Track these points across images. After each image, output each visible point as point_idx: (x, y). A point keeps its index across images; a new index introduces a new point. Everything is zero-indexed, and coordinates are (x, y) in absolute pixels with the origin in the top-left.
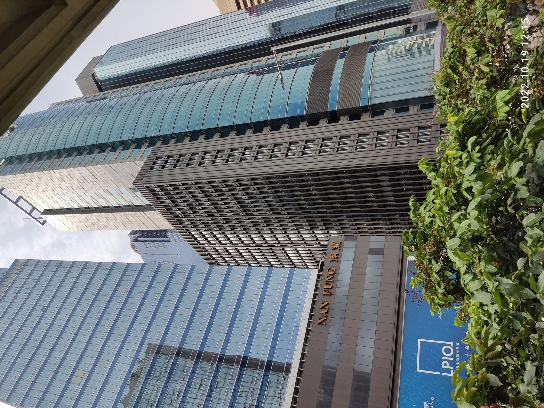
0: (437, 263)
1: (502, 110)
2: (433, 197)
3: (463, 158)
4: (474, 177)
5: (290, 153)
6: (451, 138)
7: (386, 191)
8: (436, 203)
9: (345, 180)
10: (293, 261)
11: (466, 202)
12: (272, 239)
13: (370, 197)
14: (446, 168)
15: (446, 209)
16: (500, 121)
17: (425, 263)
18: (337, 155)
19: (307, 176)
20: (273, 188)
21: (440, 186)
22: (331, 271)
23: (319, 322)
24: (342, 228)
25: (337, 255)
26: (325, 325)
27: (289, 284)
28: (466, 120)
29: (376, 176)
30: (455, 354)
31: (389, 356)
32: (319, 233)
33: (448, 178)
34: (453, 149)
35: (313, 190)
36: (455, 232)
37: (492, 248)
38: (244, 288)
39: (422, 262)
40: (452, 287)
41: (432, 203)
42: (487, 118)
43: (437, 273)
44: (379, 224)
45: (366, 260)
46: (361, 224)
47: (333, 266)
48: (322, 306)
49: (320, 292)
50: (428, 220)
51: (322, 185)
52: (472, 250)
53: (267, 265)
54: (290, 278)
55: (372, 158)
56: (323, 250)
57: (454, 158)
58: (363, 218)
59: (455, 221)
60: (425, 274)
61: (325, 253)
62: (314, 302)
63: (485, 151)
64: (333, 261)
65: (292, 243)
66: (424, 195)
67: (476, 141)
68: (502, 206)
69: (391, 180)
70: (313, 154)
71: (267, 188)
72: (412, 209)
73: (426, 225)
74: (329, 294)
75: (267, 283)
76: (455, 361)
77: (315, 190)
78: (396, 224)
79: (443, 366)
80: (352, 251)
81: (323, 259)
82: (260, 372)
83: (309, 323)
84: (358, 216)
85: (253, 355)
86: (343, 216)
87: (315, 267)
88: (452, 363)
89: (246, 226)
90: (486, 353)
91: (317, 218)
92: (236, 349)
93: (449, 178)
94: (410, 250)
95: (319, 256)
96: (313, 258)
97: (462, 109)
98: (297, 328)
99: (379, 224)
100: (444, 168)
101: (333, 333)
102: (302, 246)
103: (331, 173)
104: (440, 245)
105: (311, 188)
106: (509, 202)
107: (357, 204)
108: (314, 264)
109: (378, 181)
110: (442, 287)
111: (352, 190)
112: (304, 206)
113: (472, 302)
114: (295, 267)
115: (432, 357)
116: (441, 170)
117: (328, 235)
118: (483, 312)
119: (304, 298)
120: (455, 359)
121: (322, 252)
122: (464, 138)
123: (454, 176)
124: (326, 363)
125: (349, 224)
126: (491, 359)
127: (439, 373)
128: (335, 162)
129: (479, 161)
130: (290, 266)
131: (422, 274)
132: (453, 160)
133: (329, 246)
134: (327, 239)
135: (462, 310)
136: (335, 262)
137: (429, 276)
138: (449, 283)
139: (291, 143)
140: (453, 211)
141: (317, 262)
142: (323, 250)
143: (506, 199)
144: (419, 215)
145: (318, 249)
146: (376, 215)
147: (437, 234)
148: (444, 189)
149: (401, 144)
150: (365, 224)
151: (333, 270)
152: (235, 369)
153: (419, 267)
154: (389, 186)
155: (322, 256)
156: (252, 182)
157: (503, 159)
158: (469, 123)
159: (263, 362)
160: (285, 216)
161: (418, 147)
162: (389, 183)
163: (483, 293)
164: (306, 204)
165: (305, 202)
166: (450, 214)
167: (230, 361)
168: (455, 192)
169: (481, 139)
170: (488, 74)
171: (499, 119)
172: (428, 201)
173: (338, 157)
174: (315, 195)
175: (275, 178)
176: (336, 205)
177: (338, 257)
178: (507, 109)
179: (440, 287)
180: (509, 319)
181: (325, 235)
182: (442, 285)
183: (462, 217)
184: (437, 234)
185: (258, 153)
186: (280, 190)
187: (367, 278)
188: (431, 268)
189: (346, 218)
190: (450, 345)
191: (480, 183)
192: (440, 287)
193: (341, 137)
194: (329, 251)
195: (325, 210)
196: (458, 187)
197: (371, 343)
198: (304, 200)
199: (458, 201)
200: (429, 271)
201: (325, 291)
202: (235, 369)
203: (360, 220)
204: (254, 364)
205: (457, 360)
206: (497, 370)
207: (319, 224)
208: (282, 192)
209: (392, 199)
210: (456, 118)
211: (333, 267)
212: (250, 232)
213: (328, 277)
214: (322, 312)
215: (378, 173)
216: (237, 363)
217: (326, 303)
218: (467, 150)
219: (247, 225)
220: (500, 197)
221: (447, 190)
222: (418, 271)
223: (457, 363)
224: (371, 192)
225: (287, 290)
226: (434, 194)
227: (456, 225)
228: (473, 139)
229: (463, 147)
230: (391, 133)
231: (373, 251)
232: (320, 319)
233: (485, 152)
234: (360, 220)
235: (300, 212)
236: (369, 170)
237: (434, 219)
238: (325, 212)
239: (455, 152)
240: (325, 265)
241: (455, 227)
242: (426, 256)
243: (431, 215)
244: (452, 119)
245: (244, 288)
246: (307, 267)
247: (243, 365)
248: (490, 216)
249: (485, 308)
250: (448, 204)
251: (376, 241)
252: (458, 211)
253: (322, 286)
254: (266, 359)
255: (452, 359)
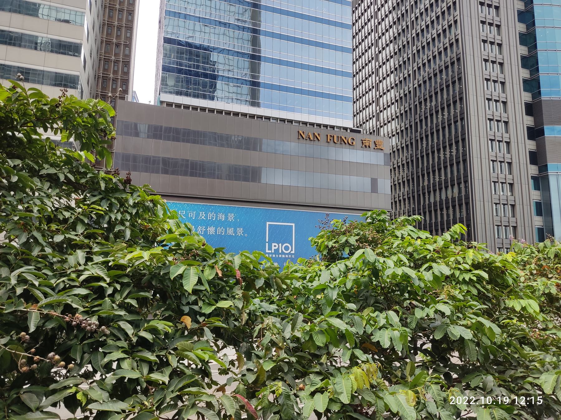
0: (357, 241)
1: (516, 304)
2: (424, 237)
3: (464, 265)
4: (437, 273)
5: (491, 84)
6: (487, 256)
7: (440, 194)
8: (417, 240)
9: (454, 151)
10: (361, 100)
11: (417, 267)
12: (385, 72)
13: (434, 178)
14: (454, 250)
15: (410, 249)
16: (504, 301)
17: (355, 230)
18: (486, 139)
19: (461, 107)
20: (447, 67)
21: (435, 245)
22: (352, 141)
23: (301, 132)
24: (398, 150)
25: (369, 147)
26: (299, 138)
27: (336, 97)
28: (506, 270)
29: (459, 184)
30: (283, 253)
31: (277, 198)
32: (394, 125)
33: (443, 253)
34: (475, 256)
35: (443, 115)
36: (388, 256)
37: (367, 285)
38: (329, 47)
39: (356, 228)
40: (335, 253)
41: (417, 236)
42: (508, 289)
43: (347, 241)
44: (404, 187)
45: (366, 177)
46: (404, 170)
47: (357, 143)
48: (316, 134)
49: (330, 131)
50: (398, 233)
51: (449, 125)
52: (366, 269)
53: (355, 71)
54: (342, 98)
55: (480, 178)
56: (374, 131)
57: (465, 258)
58: (410, 170)
59: (398, 257)
60: (345, 231)
61: (371, 133)
62: (319, 125)
63: (471, 286)
64: (363, 143)
65: (381, 96)
66: (425, 229)
67: (483, 278)
68: (409, 296)
69: (453, 199)
70: (488, 112)
71: (446, 59)
72: (410, 218)
73: (393, 232)
74: (329, 141)
75: (335, 72)
76: (279, 254)
77: (443, 118)
78: (405, 204)
79: (273, 244)
80: (374, 162)
81: (365, 132)
82: (248, 75)
83: (299, 122)
84: (413, 166)
85: (264, 66)
86: (412, 150)
87: (355, 124)
88: (277, 251)
89: (399, 39)
90: (280, 278)
91: (410, 122)
92: (268, 47)
93: (443, 253)
94: (368, 217)
95: (368, 127)
96: (364, 121)
97: (525, 269)
98: (293, 110)
99: (404, 187)
100: (455, 248)
101: (293, 147)
102: (378, 108)
103: (463, 134)
104: (374, 243)
105: (446, 113)
106: (414, 302)
107: (425, 164)
108: (358, 122)
109: (453, 186)
110: (334, 245)
111: (442, 158)
112: (423, 107)
113: (323, 268)
114: (354, 102)
115: (281, 235)
116: (453, 246)
117: (390, 135)
118: (313, 276)
119: (322, 115)
120: (280, 254)
121: (371, 131)
122: (487, 267)
123: (444, 257)
124: (264, 141)
125: (404, 157)
126: (276, 282)
127: (267, 241)
128: (478, 138)
129: (461, 279)
130: (355, 97)
131: (345, 228)
132: (463, 256)
133: (378, 138)
134: (386, 134)
135: (316, 261)
136: (361, 144)
137: (344, 234)
138: (339, 250)
139: (503, 84)
140: (408, 256)
141: (361, 125)
142: (374, 131)
143: (417, 300)
144: (403, 226)
145: (375, 126)
146: (413, 184)
147: (385, 241)
148: (431, 248)
149: (496, 209)
150: (403, 174)
151: (353, 143)
152: (248, 49)
153: (351, 225)
154: (447, 197)
155: (368, 130)
156: (454, 40)
157: (460, 300)
158: (503, 272)
159: (258, 77)
160: (411, 85)
161: (492, 226)
162: (450, 197)
163: (329, 278)
164: (426, 109)
165: (428, 107)
166: (406, 253)
167: (255, 42)
168: (428, 257)
169: (485, 283)
170: (71, 217)
171: (506, 301)
172: (419, 233)
173: (484, 141)
174: (437, 118)
175: (459, 69)
176: (424, 142)
177: (367, 147)
178: (518, 309)
179: (335, 243)
180: (306, 294)
181: (390, 132)
182: (337, 245)
183: (402, 263)
184: (385, 241)
185: (492, 43)
186: (444, 76)
187: (346, 177)
188: (351, 235)
189: (409, 153)
190: (292, 250)
191: (431, 279)
192: (335, 243)
193: (508, 143)
194: (373, 138)
195: (419, 130)
196: (433, 260)
197: (286, 183)
198: (431, 106)
199: (418, 260)
200: (348, 234)
201: (331, 136)
202: (248, 49)
203: (408, 168)
204: (255, 69)
205: (280, 256)
206: (268, 285)
207: (403, 124)
208: (441, 79)
209: (432, 200)
210: (511, 260)
211: (356, 143)
212: (391, 45)
213: (345, 138)
214: (310, 134)
215: (462, 185)
216: (254, 50)
217: (319, 138)
218: (472, 269)
219: (401, 41)
220: (418, 295)
221: (430, 250)
222: (347, 225)
223: (277, 256)
224: (440, 179)
225: (329, 96)
226: (427, 238)
227: (395, 258)
228: (486, 275)
229: (477, 266)
230: (511, 198)
231: (374, 182)
232: (303, 133)
233: (470, 286)
234: (408, 168)
235: (417, 103)
236: (466, 176)
237: (400, 239)
238: (416, 131)
239: (471, 257)
240: (358, 134)
241: (393, 257)
242: (362, 231)
243: (405, 236)
244: (509, 257)
245: (329, 47)
246: (355, 116)
247: (253, 57)
248: (397, 285)
249: (317, 278)
250: (416, 250)
251: (385, 185)
252: (408, 260)
253: (336, 133)
254: (261, 80)
255: (280, 252)
